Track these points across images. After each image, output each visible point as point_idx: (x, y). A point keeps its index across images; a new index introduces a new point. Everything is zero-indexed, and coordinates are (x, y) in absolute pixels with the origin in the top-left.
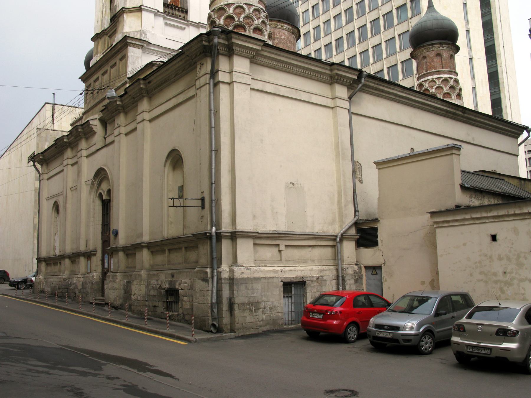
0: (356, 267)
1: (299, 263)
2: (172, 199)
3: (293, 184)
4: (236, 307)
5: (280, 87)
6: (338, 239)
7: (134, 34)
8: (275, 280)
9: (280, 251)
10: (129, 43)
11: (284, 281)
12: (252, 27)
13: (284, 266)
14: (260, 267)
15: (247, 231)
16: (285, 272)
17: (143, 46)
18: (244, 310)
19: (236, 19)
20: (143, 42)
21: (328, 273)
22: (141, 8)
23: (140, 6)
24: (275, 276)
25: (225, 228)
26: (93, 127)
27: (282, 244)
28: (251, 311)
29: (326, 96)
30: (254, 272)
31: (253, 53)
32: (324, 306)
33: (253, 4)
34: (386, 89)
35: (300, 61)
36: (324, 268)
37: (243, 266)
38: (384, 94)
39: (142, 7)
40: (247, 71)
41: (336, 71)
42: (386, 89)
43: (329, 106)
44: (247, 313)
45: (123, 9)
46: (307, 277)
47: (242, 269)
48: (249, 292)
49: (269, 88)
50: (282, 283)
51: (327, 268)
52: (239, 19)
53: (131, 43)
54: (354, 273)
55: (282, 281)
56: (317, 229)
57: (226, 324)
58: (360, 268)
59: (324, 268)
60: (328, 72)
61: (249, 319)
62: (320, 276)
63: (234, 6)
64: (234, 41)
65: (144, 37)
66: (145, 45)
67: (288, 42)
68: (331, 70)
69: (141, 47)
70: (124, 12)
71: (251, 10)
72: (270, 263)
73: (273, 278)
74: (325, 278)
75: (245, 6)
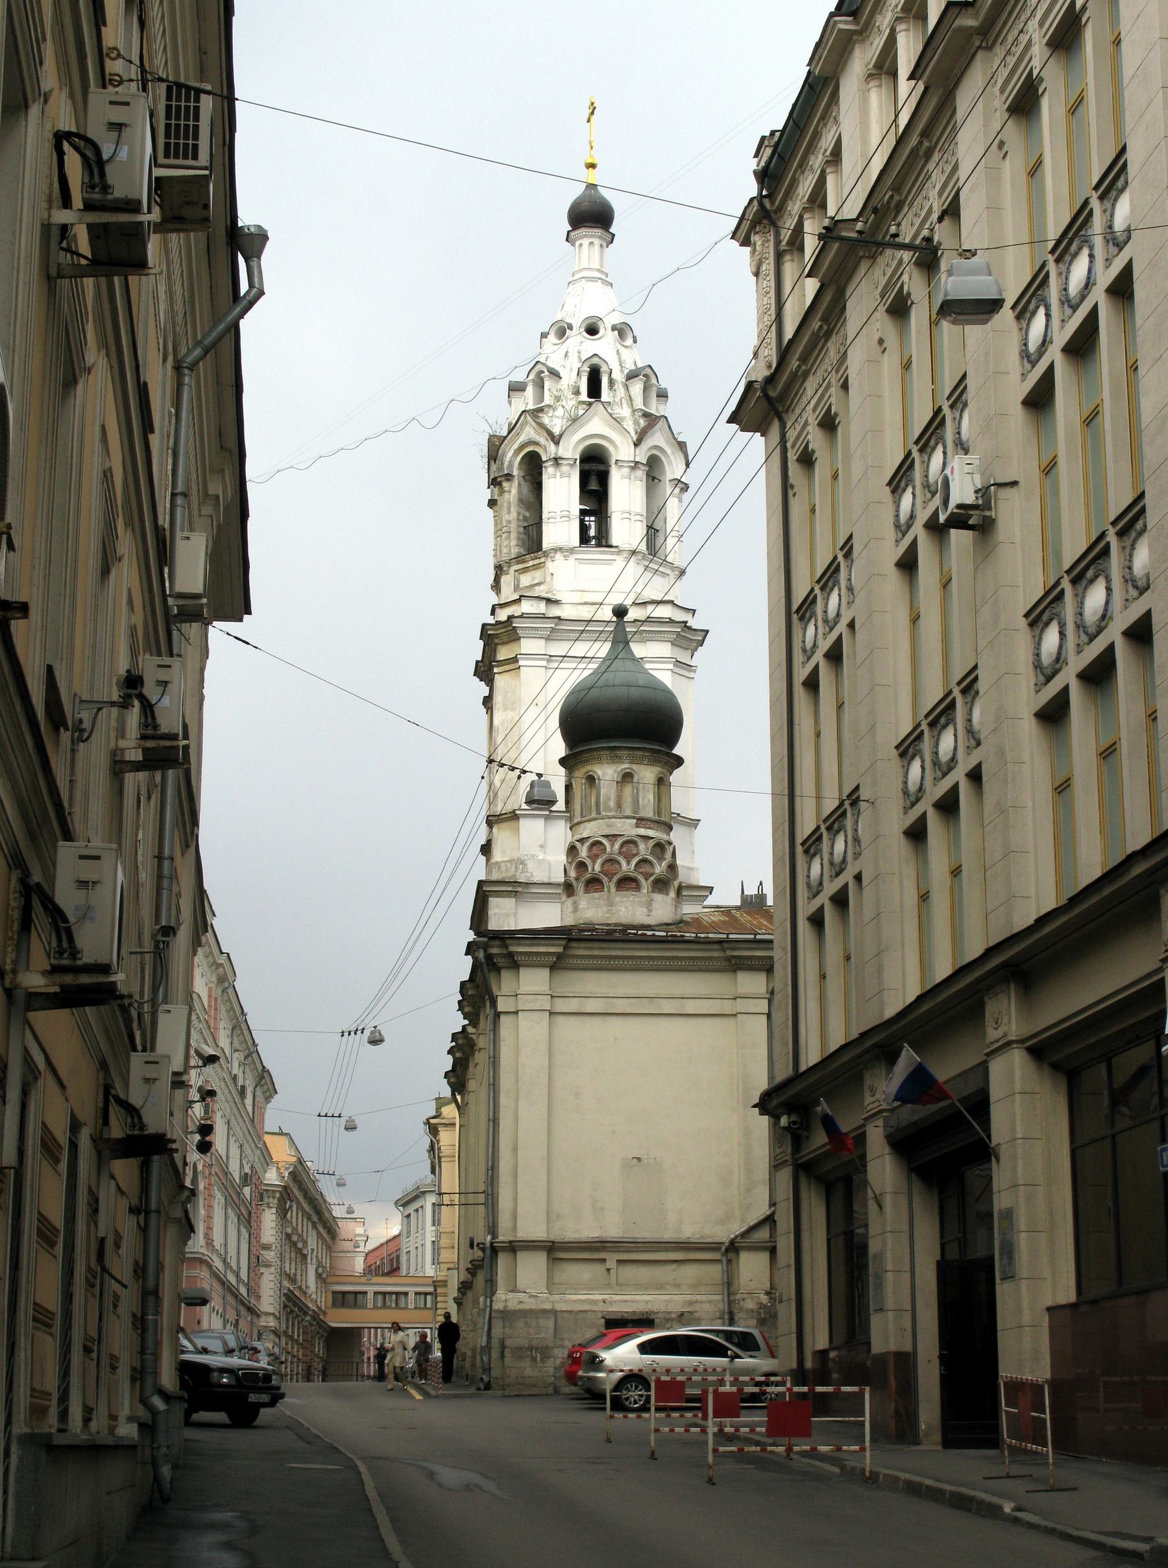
0: (764, 1299)
1: (647, 1288)
3: (639, 1159)
4: (507, 1353)
5: (615, 1000)
6: (723, 1249)
7: (506, 866)
8: (590, 1315)
9: (608, 1270)
12: (615, 879)
16: (611, 1303)
17: (516, 892)
18: (521, 1358)
21: (706, 1306)
23: (514, 811)
25: (504, 1236)
27: (612, 1259)
28: (534, 1359)
30: (542, 1302)
36: (698, 1298)
40: (545, 988)
41: (729, 953)
44: (526, 1363)
46: (657, 1313)
48: (531, 1330)
49: (591, 1006)
50: (603, 1320)
51: (704, 1298)
56: (689, 1232)
57: (497, 1378)
59: (698, 1298)
61: (528, 1372)
64: (513, 949)
66: (519, 889)
68: (724, 950)
69: (515, 894)
71: (617, 846)
72: (586, 1289)
73: (586, 1311)
74: (697, 1315)
75: (604, 841)
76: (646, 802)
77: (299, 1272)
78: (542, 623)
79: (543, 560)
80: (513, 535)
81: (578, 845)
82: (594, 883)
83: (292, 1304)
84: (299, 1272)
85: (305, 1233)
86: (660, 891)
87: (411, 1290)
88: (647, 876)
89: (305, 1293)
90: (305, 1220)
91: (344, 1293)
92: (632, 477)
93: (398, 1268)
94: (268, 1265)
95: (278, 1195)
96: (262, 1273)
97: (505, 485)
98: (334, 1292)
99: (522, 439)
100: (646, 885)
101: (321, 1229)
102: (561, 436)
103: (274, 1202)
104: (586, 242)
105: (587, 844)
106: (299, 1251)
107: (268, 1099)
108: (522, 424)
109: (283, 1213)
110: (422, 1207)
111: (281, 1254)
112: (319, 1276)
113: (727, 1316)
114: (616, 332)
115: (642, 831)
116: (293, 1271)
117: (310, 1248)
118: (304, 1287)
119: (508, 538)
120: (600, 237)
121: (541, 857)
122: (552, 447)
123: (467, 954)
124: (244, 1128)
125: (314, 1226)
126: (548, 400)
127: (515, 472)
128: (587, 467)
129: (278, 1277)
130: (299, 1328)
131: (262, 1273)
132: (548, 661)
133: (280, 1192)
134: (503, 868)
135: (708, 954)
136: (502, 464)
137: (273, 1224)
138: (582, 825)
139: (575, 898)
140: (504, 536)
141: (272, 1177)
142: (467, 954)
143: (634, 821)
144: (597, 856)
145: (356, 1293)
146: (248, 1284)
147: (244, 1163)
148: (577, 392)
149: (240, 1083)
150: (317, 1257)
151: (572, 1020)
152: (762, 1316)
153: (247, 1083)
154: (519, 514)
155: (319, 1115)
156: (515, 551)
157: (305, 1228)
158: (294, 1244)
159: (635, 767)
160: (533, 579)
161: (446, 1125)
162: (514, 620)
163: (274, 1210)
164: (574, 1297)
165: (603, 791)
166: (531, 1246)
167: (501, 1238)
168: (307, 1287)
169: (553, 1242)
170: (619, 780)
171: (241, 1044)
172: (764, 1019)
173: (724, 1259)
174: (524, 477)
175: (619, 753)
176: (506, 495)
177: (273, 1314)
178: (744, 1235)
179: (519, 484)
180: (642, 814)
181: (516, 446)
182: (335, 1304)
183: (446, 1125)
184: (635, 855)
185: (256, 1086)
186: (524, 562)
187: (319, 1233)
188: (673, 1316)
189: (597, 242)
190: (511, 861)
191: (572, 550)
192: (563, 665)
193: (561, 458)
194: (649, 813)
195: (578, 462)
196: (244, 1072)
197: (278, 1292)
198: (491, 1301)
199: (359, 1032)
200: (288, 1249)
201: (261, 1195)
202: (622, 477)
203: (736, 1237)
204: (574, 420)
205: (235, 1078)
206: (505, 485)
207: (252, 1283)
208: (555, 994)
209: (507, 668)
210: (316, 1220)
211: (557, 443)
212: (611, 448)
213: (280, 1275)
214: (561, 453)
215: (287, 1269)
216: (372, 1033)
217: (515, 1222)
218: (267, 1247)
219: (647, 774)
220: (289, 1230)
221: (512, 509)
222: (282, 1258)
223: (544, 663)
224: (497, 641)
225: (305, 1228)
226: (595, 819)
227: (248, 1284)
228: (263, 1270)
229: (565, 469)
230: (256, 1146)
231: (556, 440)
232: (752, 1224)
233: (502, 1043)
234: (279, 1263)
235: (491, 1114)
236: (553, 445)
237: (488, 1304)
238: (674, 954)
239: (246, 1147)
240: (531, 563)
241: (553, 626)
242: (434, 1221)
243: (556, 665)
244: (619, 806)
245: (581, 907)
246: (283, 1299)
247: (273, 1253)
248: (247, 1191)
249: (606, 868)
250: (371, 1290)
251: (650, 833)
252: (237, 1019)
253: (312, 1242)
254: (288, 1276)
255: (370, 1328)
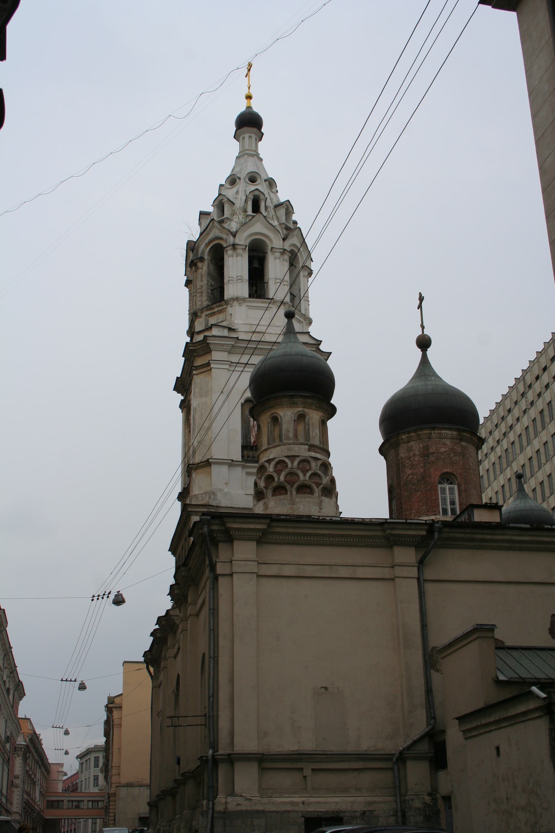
0: (428, 799)
2: (170, 717)
3: (326, 688)
5: (304, 567)
6: (394, 759)
7: (202, 497)
9: (305, 777)
10: (191, 511)
11: (306, 816)
12: (295, 486)
13: (309, 796)
14: (271, 797)
15: (246, 752)
16: (309, 804)
19: (276, 479)
20: (209, 507)
22: (209, 462)
23: (208, 460)
24: (292, 810)
26: (175, 618)
29: (380, 565)
31: (258, 534)
32: (4, 784)
33: (299, 455)
34: (488, 537)
35: (332, 529)
36: (376, 799)
37: (241, 796)
38: (489, 544)
39: (210, 460)
40: (253, 556)
41: (388, 532)
42: (488, 537)
43: (386, 577)
45: (190, 466)
46: (345, 812)
47: (239, 800)
49: (288, 571)
50: (303, 819)
52: (279, 479)
53: (194, 512)
54: (425, 807)
55: (303, 816)
56: (366, 746)
58: (435, 800)
59: (376, 799)
60: (379, 534)
62: (367, 811)
63: (275, 462)
64: (229, 525)
65: (214, 499)
67: (452, 455)
68: (384, 531)
70: (192, 469)
71: (296, 463)
73: (289, 812)
75: (287, 460)
76: (314, 434)
77: (32, 790)
78: (227, 341)
79: (225, 307)
80: (205, 294)
81: (267, 464)
82: (280, 490)
83: (28, 807)
84: (32, 790)
85: (35, 771)
86: (326, 496)
87: (86, 799)
88: (318, 485)
89: (34, 801)
90: (36, 764)
91: (52, 801)
92: (281, 259)
93: (77, 789)
94: (17, 787)
95: (23, 750)
96: (14, 791)
97: (200, 264)
98: (48, 801)
99: (211, 236)
100: (317, 491)
101: (42, 768)
102: (236, 232)
103: (21, 753)
104: (247, 136)
105: (273, 463)
106: (32, 780)
107: (21, 698)
108: (211, 228)
109: (25, 759)
110: (89, 759)
111: (23, 781)
112: (41, 792)
113: (399, 814)
114: (267, 182)
115: (313, 454)
116: (29, 790)
117: (37, 778)
118: (34, 798)
119: (201, 296)
120: (255, 133)
121: (226, 490)
122: (231, 239)
123: (143, 657)
124: (8, 711)
125: (40, 767)
126: (227, 213)
127: (206, 257)
128: (252, 254)
129: (22, 793)
130: (30, 820)
131: (14, 791)
132: (230, 366)
133: (24, 748)
134: (200, 498)
135: (373, 533)
136: (197, 252)
137: (21, 765)
138: (269, 451)
139: (265, 500)
140: (198, 295)
141: (21, 741)
142: (143, 657)
143: (307, 447)
144: (281, 471)
145: (58, 801)
146: (7, 796)
147: (7, 730)
148: (245, 211)
149: (7, 686)
150: (40, 783)
151: (273, 581)
152: (427, 813)
153: (11, 687)
154: (208, 281)
155: (62, 680)
156: (205, 303)
157: (35, 768)
158: (30, 776)
159: (306, 410)
160: (218, 319)
161: (116, 708)
162: (208, 338)
163: (21, 758)
164: (280, 800)
165: (284, 427)
166: (247, 757)
167: (221, 752)
168: (35, 798)
169: (263, 754)
170: (296, 419)
171: (8, 665)
172: (415, 581)
173: (396, 767)
174: (211, 261)
175: (295, 400)
176: (200, 271)
177: (18, 813)
178: (409, 748)
179: (208, 264)
180: (312, 442)
181: (207, 241)
182: (48, 807)
183: (116, 708)
184: (308, 470)
185: (15, 690)
186: (212, 309)
187: (42, 771)
188: (358, 814)
189: (253, 136)
190: (205, 493)
191: (244, 299)
192: (237, 369)
193: (237, 244)
194: (316, 442)
195: (247, 248)
196: (9, 681)
197: (21, 801)
198: (213, 804)
199: (105, 597)
200: (27, 778)
201: (15, 749)
202: (275, 258)
203: (404, 749)
204: (243, 225)
205: (4, 682)
206: (200, 264)
207: (8, 796)
208: (260, 562)
209: (202, 370)
210: (41, 764)
211: (234, 236)
212: (268, 242)
213: (23, 792)
214: (237, 241)
215: (26, 789)
216: (116, 596)
217: (232, 739)
218: (17, 777)
219: (314, 416)
220: (28, 768)
221: (204, 279)
222: (24, 782)
223: (227, 367)
224: (195, 354)
225: (35, 768)
226: (279, 446)
227: (7, 796)
228: (14, 789)
229: (240, 251)
230: (14, 722)
231: (234, 235)
232: (415, 738)
233: (220, 598)
234: (22, 785)
235: (212, 653)
236: (231, 237)
237: (211, 806)
238: (344, 532)
239: (9, 722)
240: (216, 310)
241: (233, 343)
242: (95, 765)
243: (232, 369)
244: (296, 436)
245: (270, 506)
246: (24, 804)
247: (20, 780)
248: (8, 746)
249: (288, 479)
250: (65, 799)
251: (318, 456)
252: (7, 650)
253: (38, 775)
254: (26, 792)
255: (65, 819)
